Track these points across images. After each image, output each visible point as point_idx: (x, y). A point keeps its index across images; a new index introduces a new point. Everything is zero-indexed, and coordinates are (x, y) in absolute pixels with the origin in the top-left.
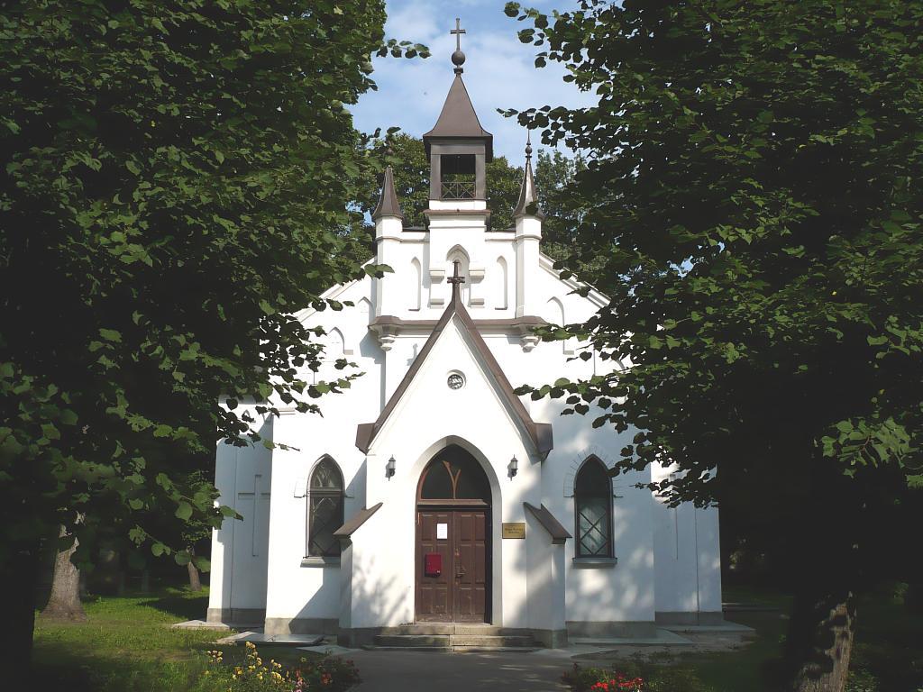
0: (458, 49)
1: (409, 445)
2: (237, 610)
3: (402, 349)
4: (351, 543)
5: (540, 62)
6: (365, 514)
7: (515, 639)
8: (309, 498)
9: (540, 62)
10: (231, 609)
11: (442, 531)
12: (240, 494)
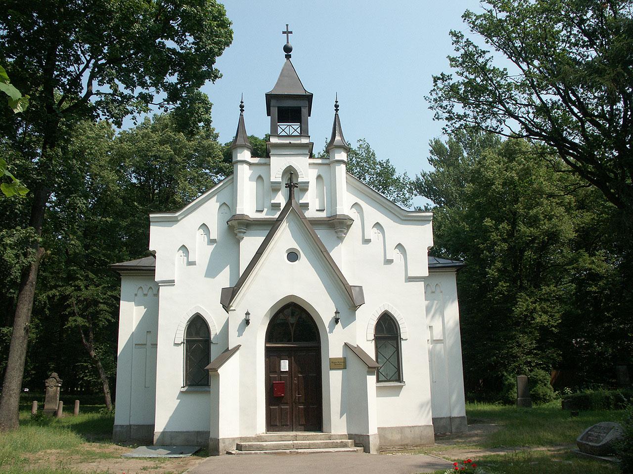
0: (288, 42)
1: (260, 300)
2: (134, 425)
3: (250, 244)
4: (218, 375)
5: (451, 75)
6: (228, 353)
7: (342, 442)
8: (185, 345)
9: (451, 75)
10: (130, 426)
11: (285, 365)
12: (136, 344)
